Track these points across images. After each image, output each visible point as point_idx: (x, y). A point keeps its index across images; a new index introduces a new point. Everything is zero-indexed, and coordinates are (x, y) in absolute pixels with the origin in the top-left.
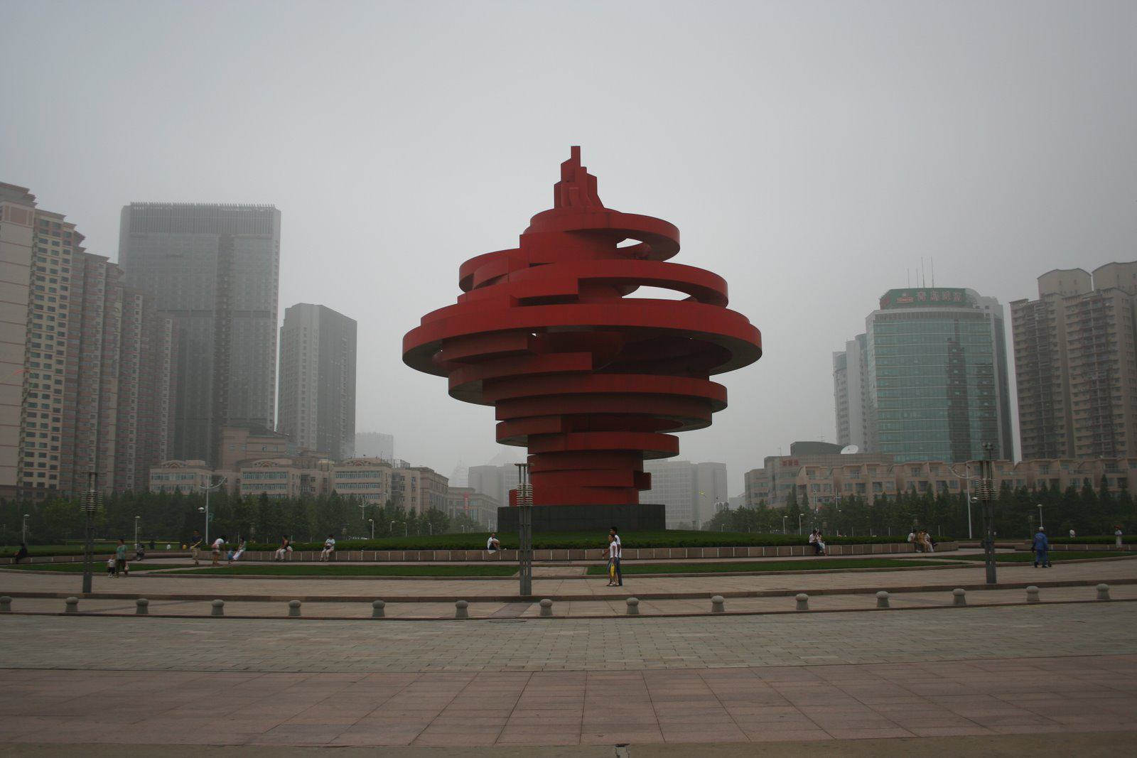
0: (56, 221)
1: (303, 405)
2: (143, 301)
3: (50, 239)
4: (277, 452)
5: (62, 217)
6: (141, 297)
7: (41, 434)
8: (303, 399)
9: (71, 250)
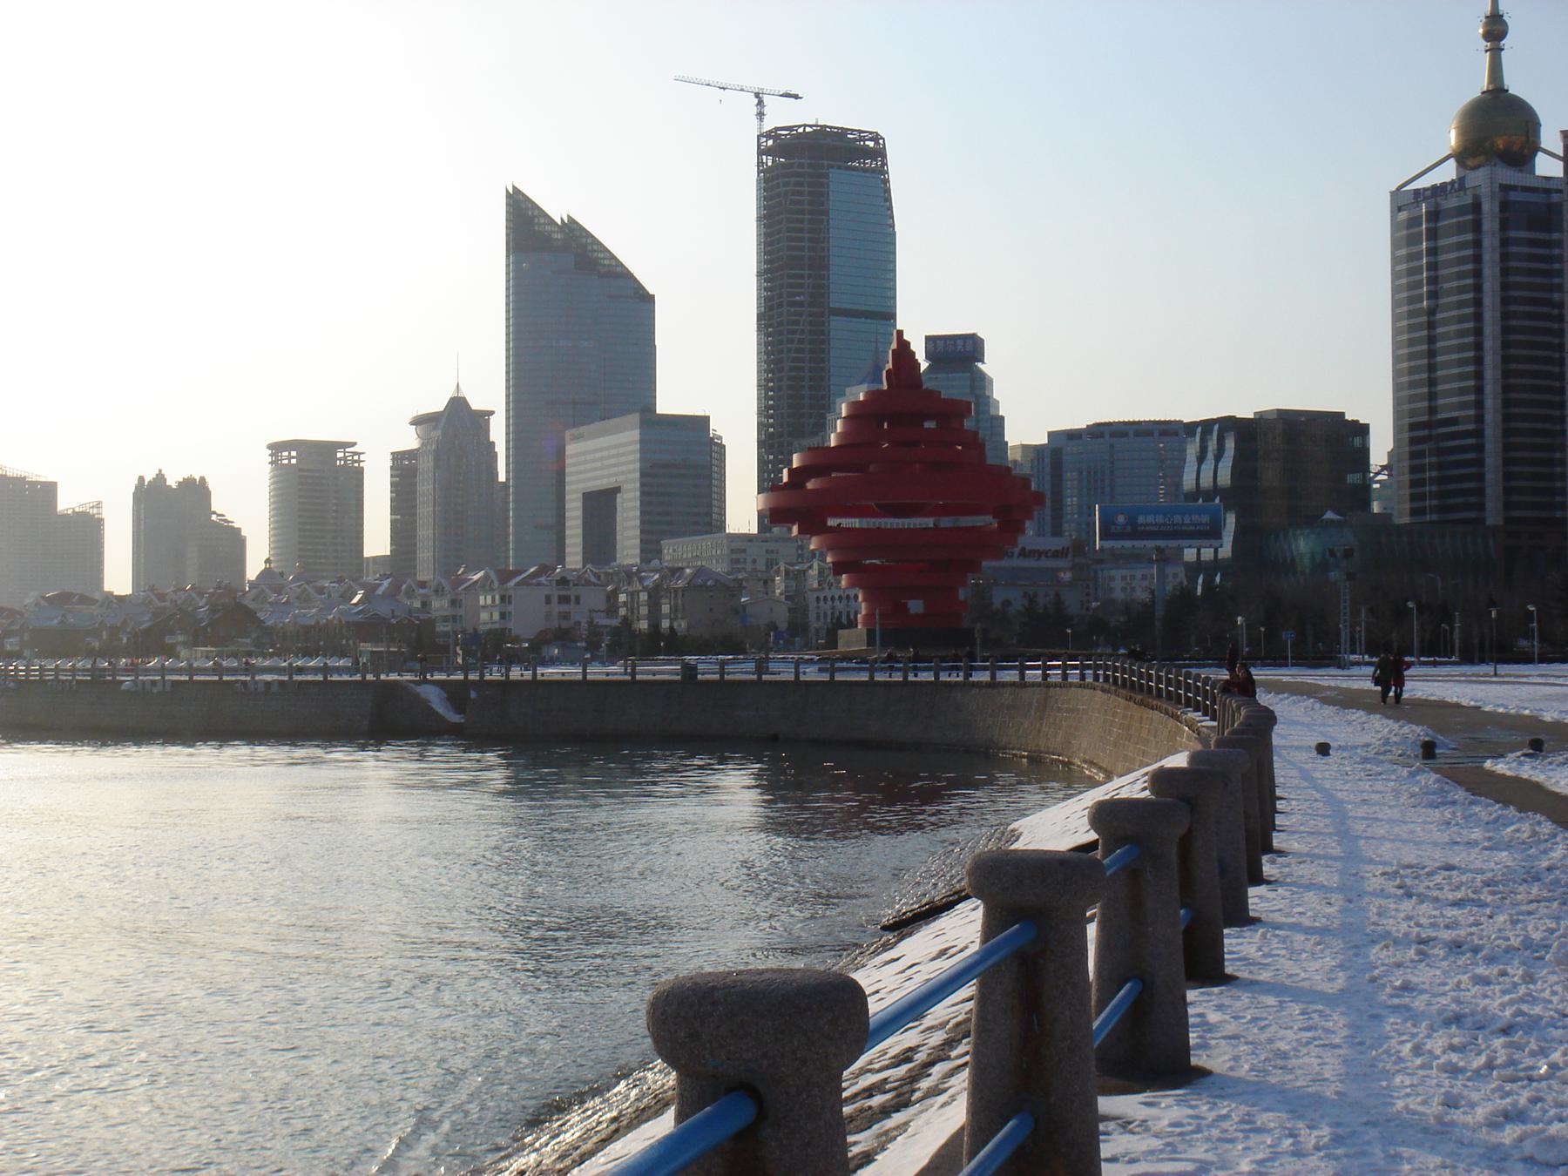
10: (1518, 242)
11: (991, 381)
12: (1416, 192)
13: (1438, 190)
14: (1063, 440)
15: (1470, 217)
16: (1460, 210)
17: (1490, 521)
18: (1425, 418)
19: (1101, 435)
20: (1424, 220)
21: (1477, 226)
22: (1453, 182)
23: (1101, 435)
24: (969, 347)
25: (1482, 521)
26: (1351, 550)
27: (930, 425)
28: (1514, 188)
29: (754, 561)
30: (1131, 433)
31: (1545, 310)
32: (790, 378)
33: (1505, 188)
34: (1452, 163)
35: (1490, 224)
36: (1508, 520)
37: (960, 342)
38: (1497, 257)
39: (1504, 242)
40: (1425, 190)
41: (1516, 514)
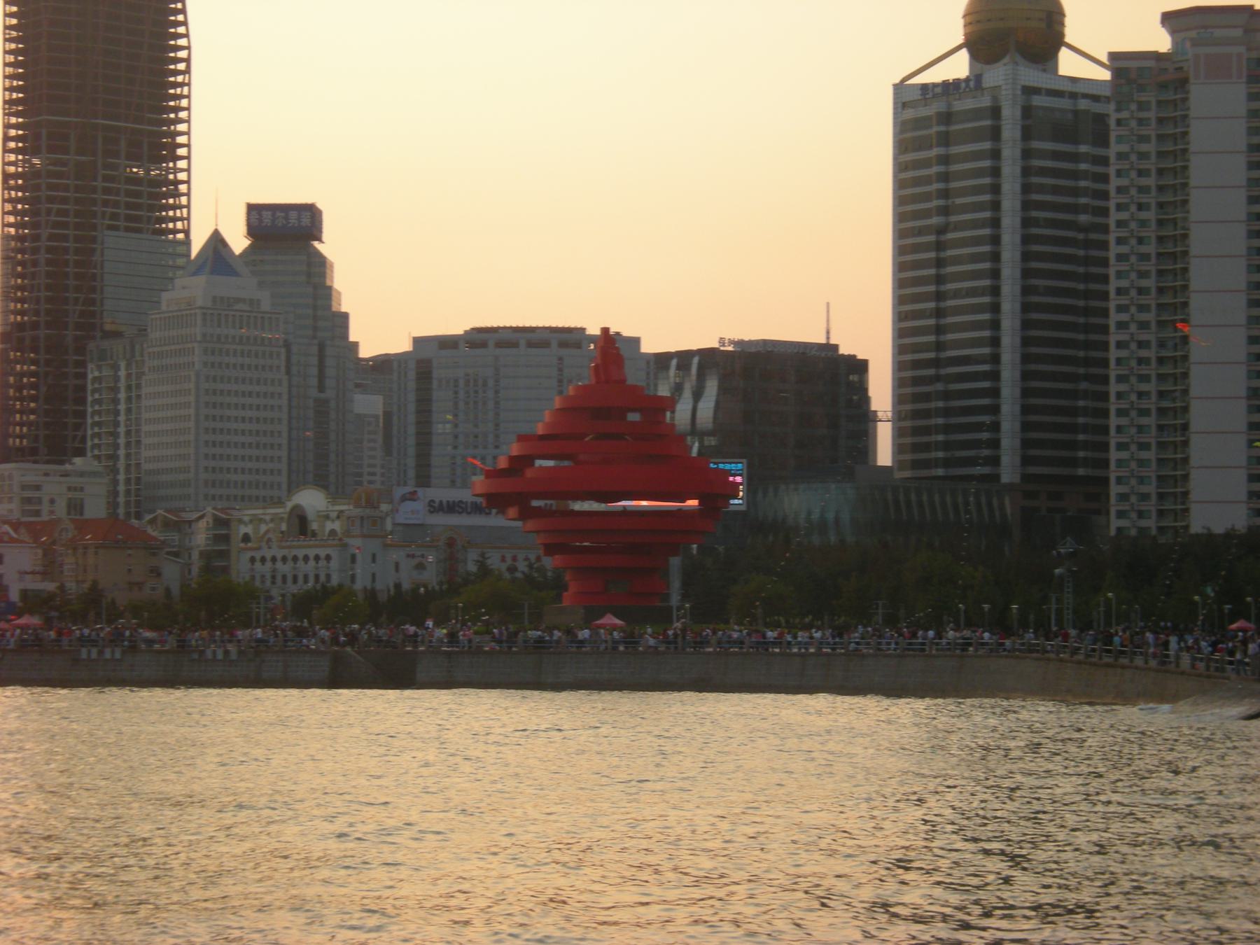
10: (1042, 154)
11: (332, 266)
12: (924, 87)
13: (950, 88)
14: (432, 356)
15: (988, 122)
16: (976, 114)
17: (1005, 479)
18: (932, 355)
19: (484, 345)
20: (930, 126)
21: (995, 134)
22: (967, 80)
23: (484, 345)
24: (306, 221)
25: (996, 478)
26: (159, 575)
27: (634, 417)
28: (1036, 91)
29: (52, 501)
30: (522, 343)
31: (1070, 234)
32: (49, 250)
33: (1029, 91)
34: (964, 55)
36: (1026, 478)
37: (293, 215)
38: (1018, 188)
39: (1027, 154)
40: (935, 85)
41: (1033, 470)
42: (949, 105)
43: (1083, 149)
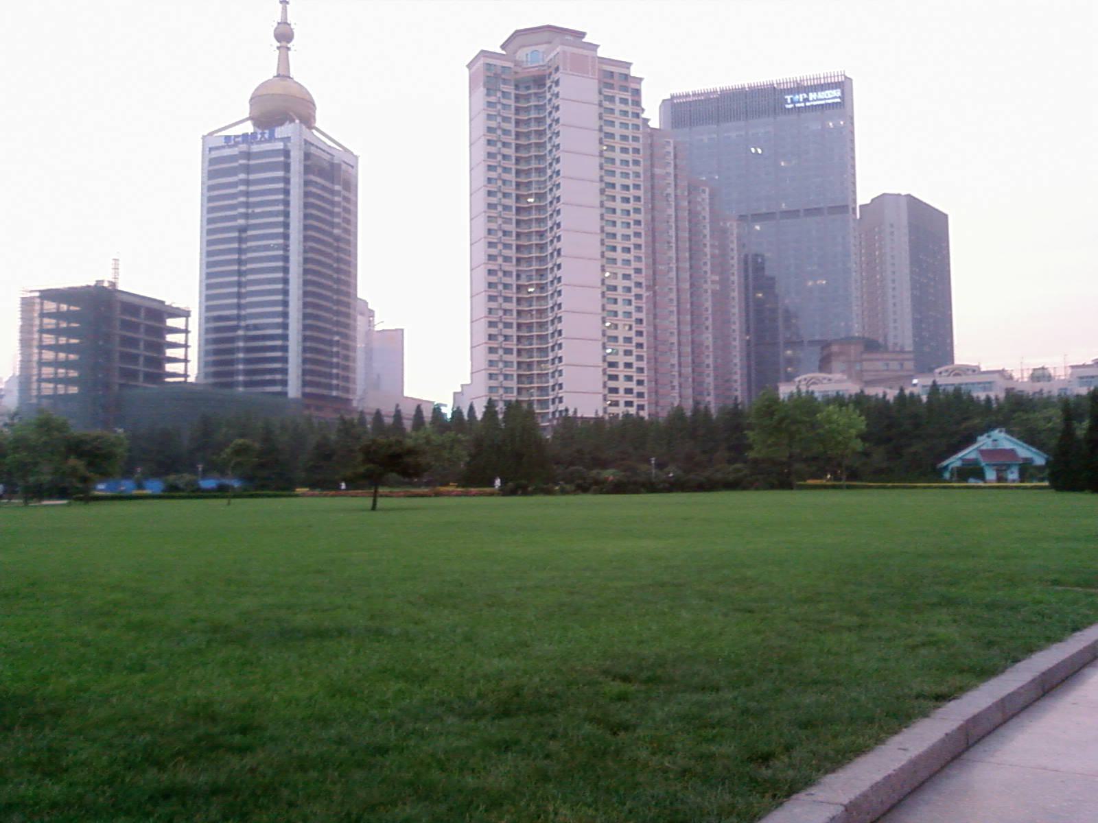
0: (624, 71)
1: (895, 328)
2: (710, 195)
3: (619, 95)
4: (887, 370)
5: (628, 65)
6: (707, 190)
7: (626, 376)
8: (895, 328)
9: (641, 160)
18: (235, 312)
35: (296, 166)
36: (305, 395)
42: (249, 148)
43: (337, 188)
